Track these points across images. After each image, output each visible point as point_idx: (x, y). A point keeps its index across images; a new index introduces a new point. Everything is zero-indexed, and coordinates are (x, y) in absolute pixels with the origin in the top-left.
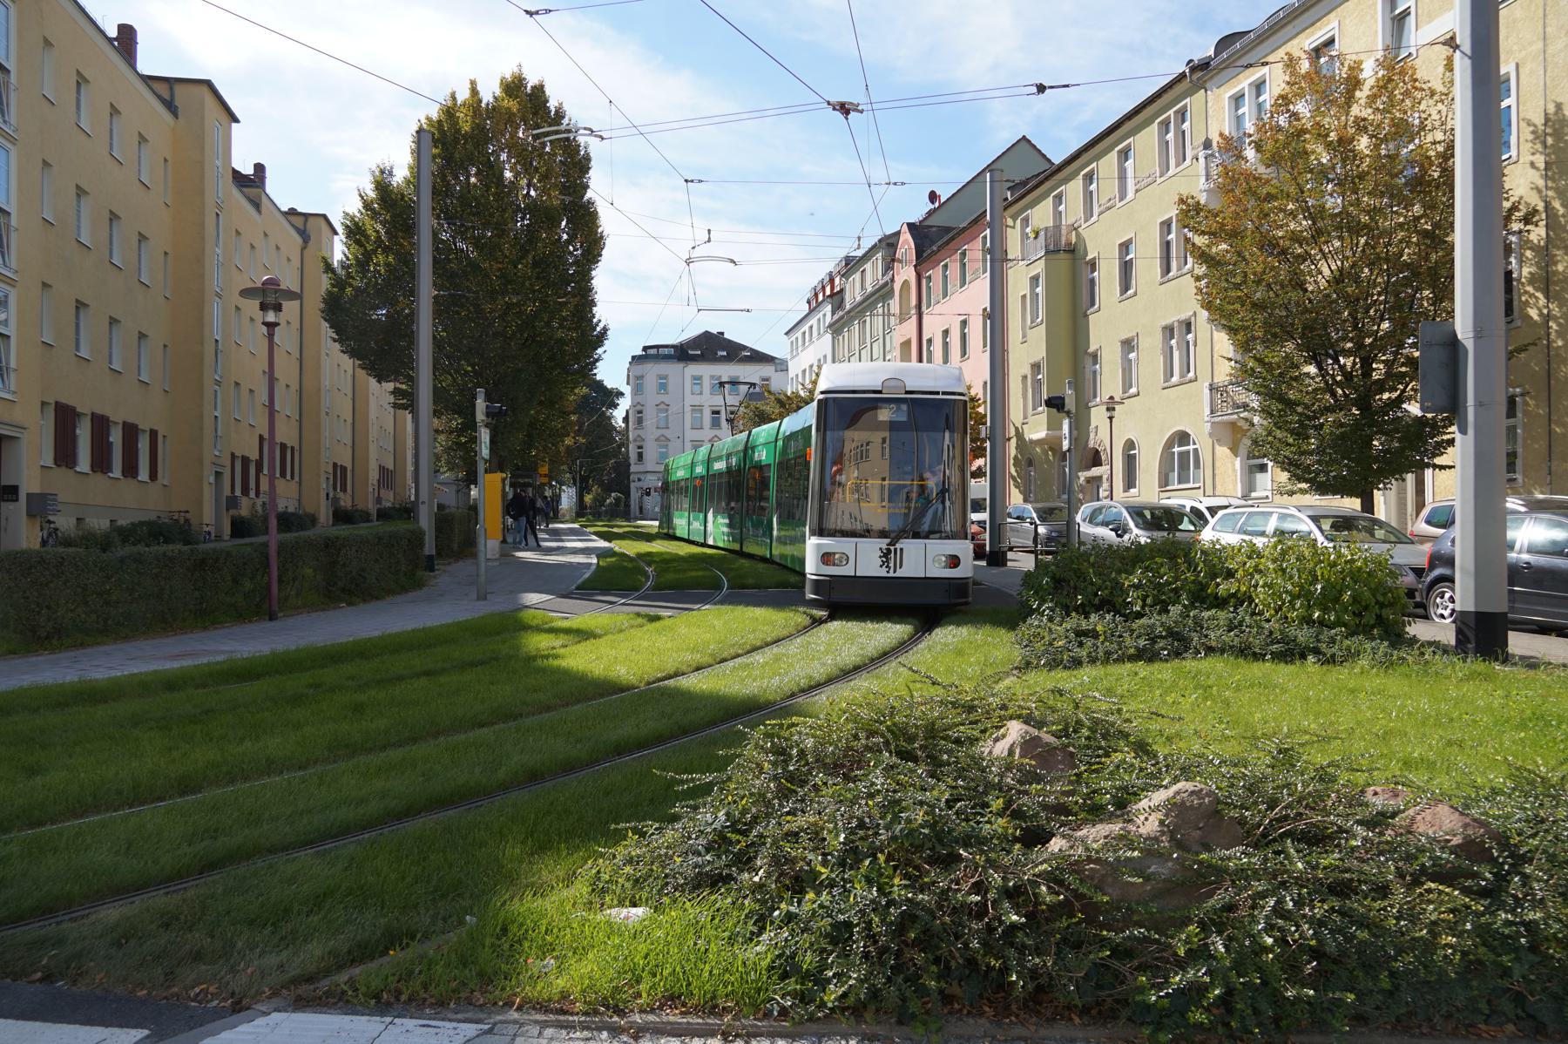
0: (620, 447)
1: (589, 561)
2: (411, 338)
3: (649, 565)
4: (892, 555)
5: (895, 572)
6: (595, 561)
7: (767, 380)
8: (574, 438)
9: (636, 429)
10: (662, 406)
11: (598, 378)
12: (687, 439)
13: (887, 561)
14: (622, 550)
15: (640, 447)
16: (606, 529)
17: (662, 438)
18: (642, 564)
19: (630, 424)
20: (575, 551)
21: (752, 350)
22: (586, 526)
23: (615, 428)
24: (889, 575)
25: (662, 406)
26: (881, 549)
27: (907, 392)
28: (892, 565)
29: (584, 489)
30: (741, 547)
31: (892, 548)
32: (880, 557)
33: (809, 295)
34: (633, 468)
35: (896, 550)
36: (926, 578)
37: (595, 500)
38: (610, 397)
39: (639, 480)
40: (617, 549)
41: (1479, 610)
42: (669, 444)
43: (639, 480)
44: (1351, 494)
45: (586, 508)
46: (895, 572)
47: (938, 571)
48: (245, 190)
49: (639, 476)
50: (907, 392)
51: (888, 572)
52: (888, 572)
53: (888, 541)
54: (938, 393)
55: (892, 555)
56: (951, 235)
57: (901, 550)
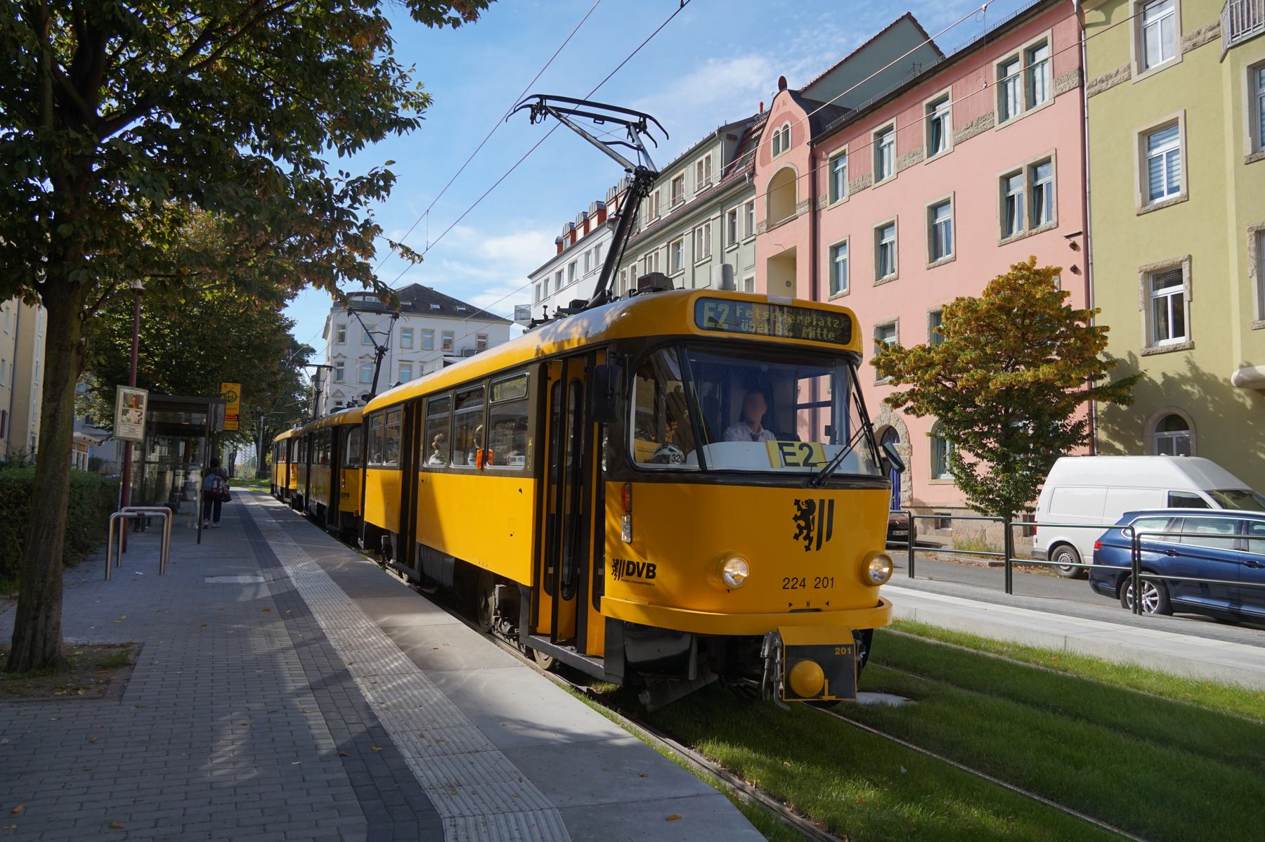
4: (816, 514)
7: (484, 338)
11: (287, 313)
13: (808, 528)
21: (467, 305)
26: (797, 502)
28: (814, 534)
32: (796, 518)
33: (560, 234)
38: (301, 353)
41: (533, 475)
44: (179, 445)
55: (816, 514)
56: (843, 118)
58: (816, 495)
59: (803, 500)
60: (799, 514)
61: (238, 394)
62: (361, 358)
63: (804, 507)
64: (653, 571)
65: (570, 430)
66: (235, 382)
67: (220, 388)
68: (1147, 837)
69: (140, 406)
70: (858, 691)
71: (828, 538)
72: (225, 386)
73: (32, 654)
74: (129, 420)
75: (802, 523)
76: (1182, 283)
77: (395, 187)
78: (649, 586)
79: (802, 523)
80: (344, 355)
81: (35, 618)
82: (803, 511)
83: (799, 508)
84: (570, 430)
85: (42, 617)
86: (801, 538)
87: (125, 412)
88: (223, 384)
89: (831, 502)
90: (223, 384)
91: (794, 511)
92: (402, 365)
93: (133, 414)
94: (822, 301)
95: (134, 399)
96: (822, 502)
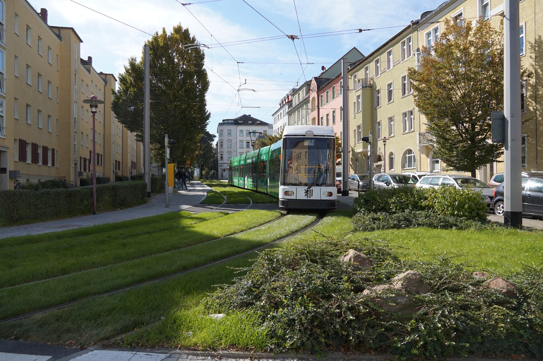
0: (215, 154)
1: (204, 194)
2: (142, 117)
3: (225, 195)
4: (309, 192)
5: (310, 198)
6: (206, 194)
7: (266, 131)
8: (199, 151)
9: (220, 148)
10: (229, 140)
11: (207, 131)
12: (238, 152)
13: (307, 194)
14: (215, 190)
15: (222, 155)
16: (210, 183)
17: (229, 152)
18: (222, 195)
19: (218, 146)
20: (199, 191)
21: (260, 121)
22: (203, 182)
23: (213, 148)
24: (308, 199)
25: (229, 140)
26: (305, 190)
27: (314, 136)
28: (309, 195)
29: (202, 169)
30: (257, 189)
31: (309, 190)
32: (305, 193)
33: (280, 102)
34: (219, 162)
35: (310, 190)
36: (321, 200)
37: (206, 173)
38: (211, 137)
39: (221, 166)
40: (214, 190)
41: (512, 211)
42: (232, 153)
43: (221, 166)
44: (468, 171)
45: (203, 176)
46: (310, 198)
47: (325, 197)
48: (85, 66)
49: (221, 165)
50: (314, 136)
51: (308, 198)
52: (308, 198)
53: (307, 187)
54: (325, 136)
55: (309, 192)
56: (329, 81)
57: (312, 190)
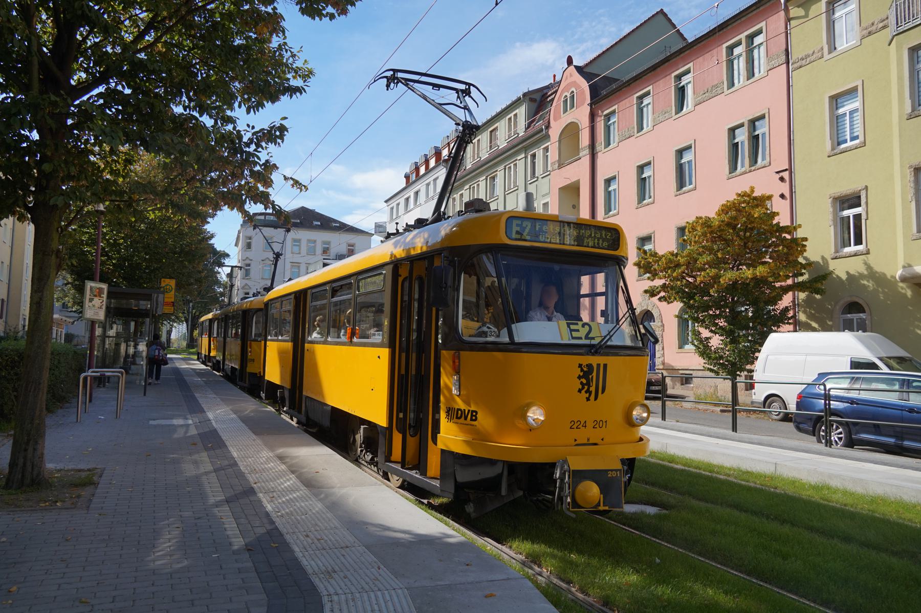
4: (594, 374)
7: (353, 246)
11: (209, 228)
13: (588, 384)
21: (340, 222)
26: (580, 366)
28: (593, 389)
32: (579, 377)
33: (408, 170)
38: (219, 257)
41: (388, 346)
44: (130, 324)
55: (594, 374)
56: (614, 86)
58: (594, 360)
59: (584, 364)
60: (582, 374)
61: (174, 287)
62: (263, 260)
63: (585, 369)
64: (475, 416)
65: (415, 313)
66: (171, 278)
67: (160, 282)
68: (835, 609)
69: (102, 295)
70: (625, 503)
71: (603, 392)
72: (164, 281)
73: (23, 476)
74: (94, 306)
75: (584, 381)
76: (860, 206)
77: (288, 136)
78: (472, 427)
79: (584, 381)
80: (251, 258)
81: (26, 450)
82: (585, 372)
83: (582, 370)
84: (415, 313)
85: (30, 449)
86: (583, 392)
87: (91, 300)
88: (163, 280)
89: (605, 366)
90: (163, 280)
91: (578, 372)
92: (293, 266)
93: (97, 301)
94: (599, 219)
95: (97, 290)
96: (599, 365)
